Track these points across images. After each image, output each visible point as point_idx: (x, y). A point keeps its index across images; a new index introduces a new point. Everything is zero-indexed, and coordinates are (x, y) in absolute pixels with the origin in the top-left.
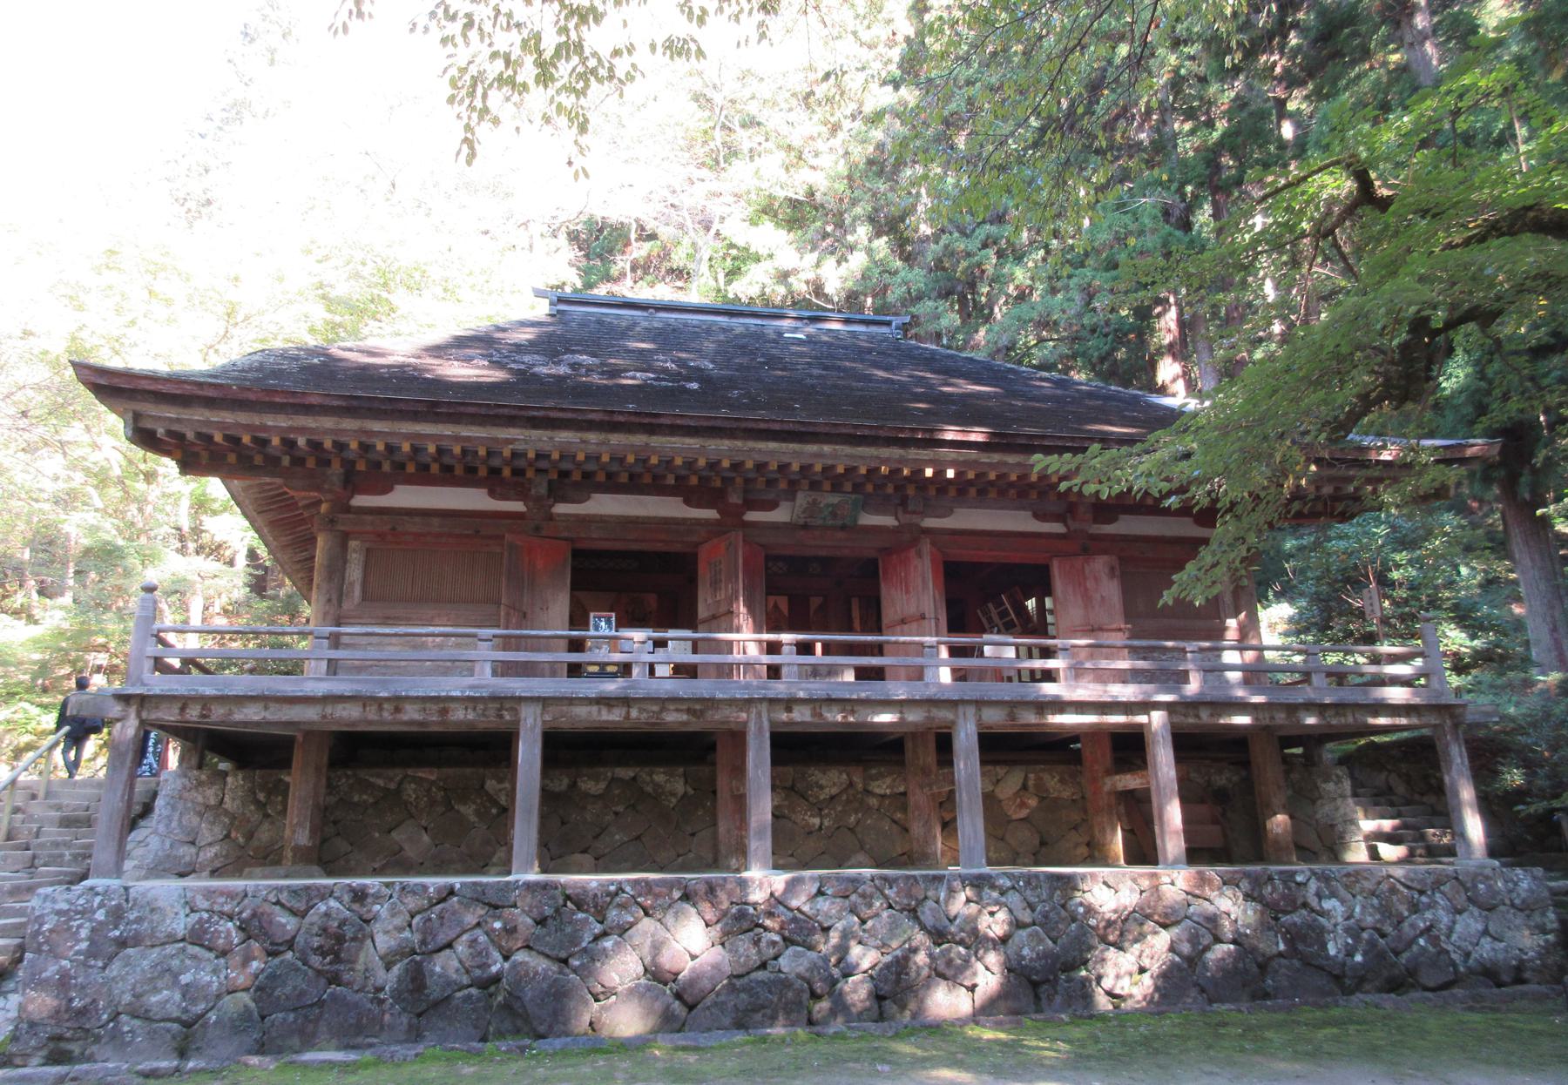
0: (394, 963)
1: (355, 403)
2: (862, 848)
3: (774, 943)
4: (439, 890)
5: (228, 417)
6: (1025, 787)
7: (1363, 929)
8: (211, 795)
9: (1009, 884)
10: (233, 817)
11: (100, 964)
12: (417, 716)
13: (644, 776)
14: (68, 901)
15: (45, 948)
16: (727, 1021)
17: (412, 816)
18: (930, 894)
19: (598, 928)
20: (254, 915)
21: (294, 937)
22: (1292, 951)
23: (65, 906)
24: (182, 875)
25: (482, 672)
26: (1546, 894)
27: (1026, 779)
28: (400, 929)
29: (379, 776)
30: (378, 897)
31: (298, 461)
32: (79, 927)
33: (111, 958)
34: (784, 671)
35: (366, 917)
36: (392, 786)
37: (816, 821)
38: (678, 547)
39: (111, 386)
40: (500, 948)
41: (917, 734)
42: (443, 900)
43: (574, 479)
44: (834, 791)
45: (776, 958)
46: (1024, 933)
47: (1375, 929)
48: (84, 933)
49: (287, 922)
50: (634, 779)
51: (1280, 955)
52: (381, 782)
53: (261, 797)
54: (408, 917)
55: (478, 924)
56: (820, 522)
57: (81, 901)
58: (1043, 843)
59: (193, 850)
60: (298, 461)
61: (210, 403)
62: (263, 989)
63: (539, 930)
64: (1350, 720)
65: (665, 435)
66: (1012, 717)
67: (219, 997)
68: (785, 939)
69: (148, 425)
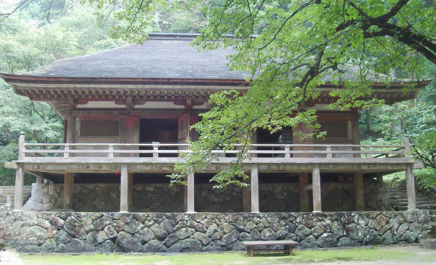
2: (231, 208)
3: (192, 231)
5: (39, 85)
6: (283, 190)
7: (370, 229)
8: (45, 190)
9: (262, 216)
12: (93, 168)
16: (178, 251)
17: (98, 197)
20: (53, 219)
26: (429, 218)
27: (284, 187)
31: (59, 96)
36: (93, 188)
37: (217, 199)
40: (116, 230)
41: (303, 174)
43: (139, 98)
49: (62, 221)
50: (162, 187)
51: (344, 236)
52: (90, 187)
53: (58, 190)
54: (92, 221)
55: (110, 224)
58: (288, 206)
59: (42, 205)
60: (59, 96)
65: (161, 85)
66: (269, 167)
67: (46, 239)
69: (19, 88)
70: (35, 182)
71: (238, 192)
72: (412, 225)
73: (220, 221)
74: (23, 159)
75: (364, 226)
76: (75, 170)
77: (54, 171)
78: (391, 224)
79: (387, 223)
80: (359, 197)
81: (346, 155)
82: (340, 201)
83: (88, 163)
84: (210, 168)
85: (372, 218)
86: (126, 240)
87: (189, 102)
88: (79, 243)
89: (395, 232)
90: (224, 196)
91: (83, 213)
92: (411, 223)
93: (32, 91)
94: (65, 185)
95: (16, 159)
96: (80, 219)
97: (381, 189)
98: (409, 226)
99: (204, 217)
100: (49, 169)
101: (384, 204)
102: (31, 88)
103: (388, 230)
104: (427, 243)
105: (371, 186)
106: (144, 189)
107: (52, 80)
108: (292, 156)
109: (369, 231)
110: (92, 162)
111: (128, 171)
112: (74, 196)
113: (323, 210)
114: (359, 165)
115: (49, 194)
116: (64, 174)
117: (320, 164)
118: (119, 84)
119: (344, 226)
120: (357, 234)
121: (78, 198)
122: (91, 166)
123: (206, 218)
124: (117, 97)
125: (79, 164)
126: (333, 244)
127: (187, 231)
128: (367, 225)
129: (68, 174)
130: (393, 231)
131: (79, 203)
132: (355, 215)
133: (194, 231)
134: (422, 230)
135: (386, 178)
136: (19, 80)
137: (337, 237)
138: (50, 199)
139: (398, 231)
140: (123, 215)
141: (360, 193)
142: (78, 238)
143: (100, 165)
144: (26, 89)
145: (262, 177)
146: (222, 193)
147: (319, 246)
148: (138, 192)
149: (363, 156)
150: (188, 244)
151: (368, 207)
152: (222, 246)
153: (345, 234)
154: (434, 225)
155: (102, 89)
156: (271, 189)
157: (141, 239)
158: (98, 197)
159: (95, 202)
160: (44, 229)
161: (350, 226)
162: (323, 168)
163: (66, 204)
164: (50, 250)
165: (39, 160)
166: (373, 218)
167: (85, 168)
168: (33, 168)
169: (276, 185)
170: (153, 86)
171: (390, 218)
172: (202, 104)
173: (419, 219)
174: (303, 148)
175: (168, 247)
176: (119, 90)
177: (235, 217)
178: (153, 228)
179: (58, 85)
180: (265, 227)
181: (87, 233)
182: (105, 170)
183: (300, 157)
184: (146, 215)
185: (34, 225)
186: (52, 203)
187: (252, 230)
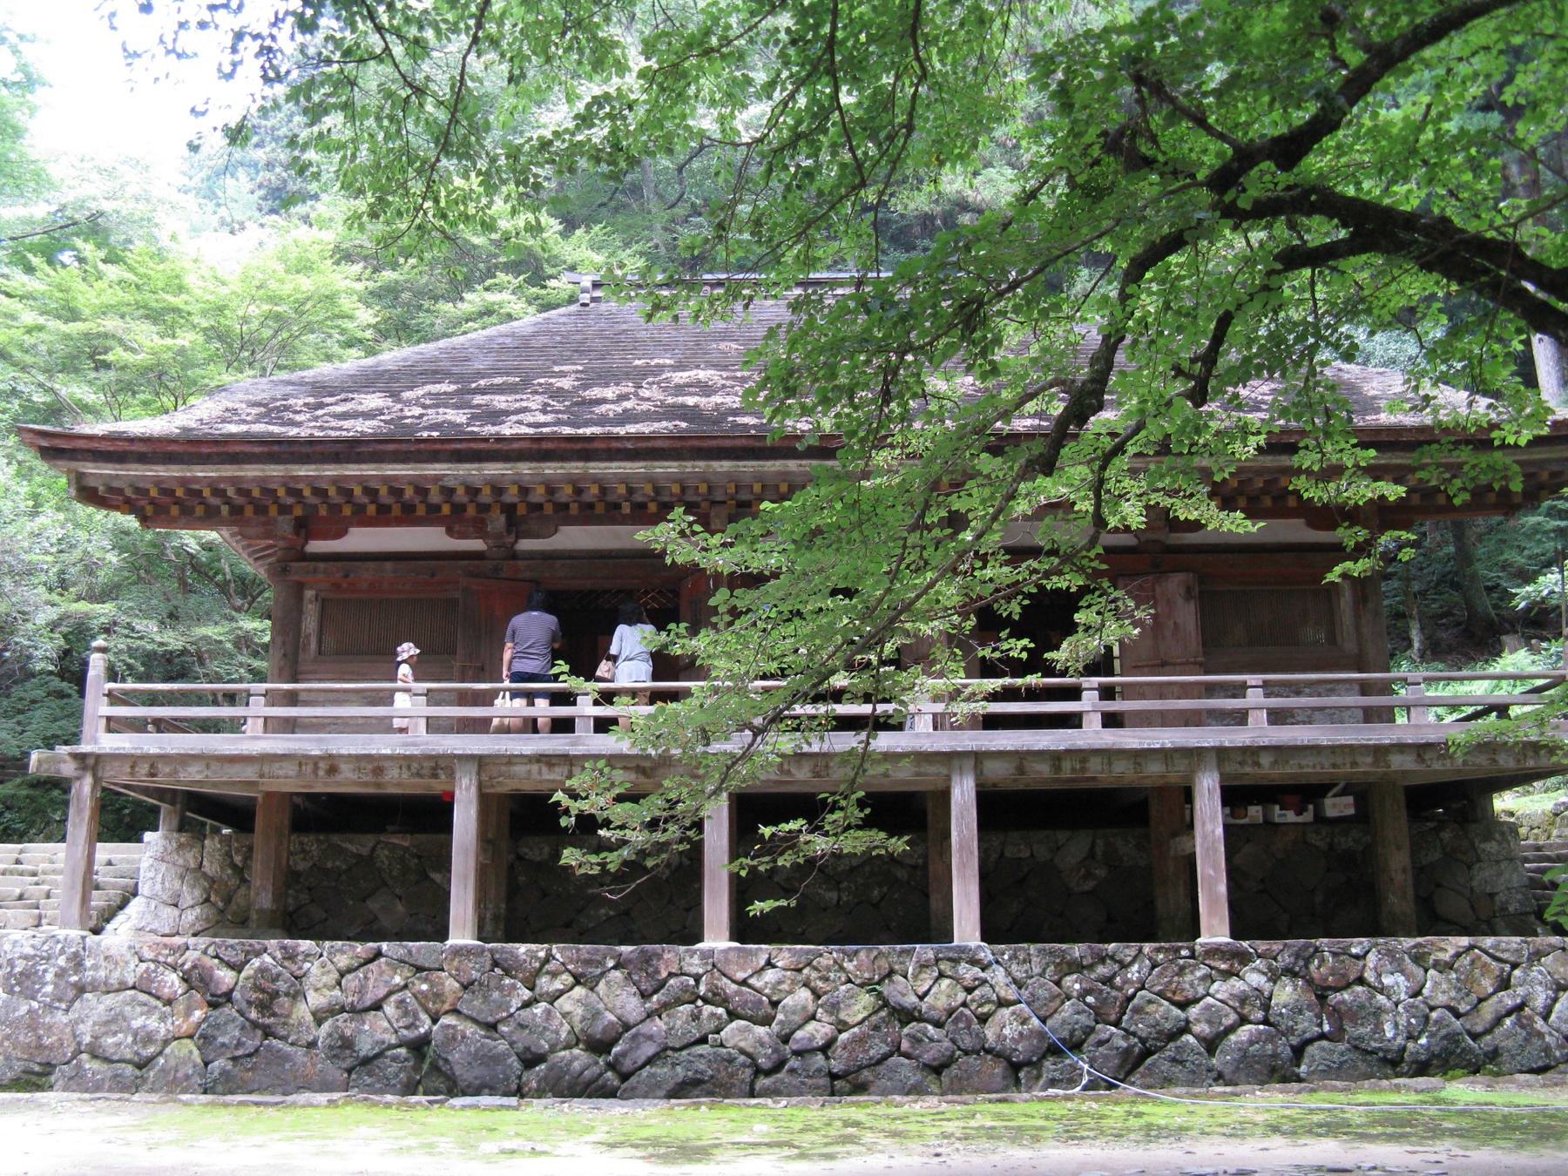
0: (326, 1019)
1: (276, 448)
5: (161, 471)
6: (1091, 855)
7: (1432, 1009)
8: (190, 858)
10: (212, 881)
11: (64, 1006)
14: (33, 946)
15: (17, 989)
16: (663, 1093)
20: (195, 967)
21: (232, 990)
23: (32, 952)
28: (331, 988)
29: (351, 842)
31: (236, 511)
32: (45, 971)
33: (72, 1002)
35: (299, 973)
36: (365, 852)
37: (834, 895)
40: (427, 1011)
41: (1163, 791)
43: (526, 512)
48: (49, 977)
49: (225, 977)
51: (1322, 1036)
52: (353, 848)
54: (336, 975)
55: (406, 986)
57: (46, 947)
59: (176, 912)
61: (169, 458)
66: (1021, 770)
67: (166, 1043)
68: (729, 1013)
69: (92, 483)
70: (156, 829)
71: (915, 867)
73: (826, 979)
74: (95, 741)
75: (1403, 996)
76: (288, 781)
77: (215, 784)
78: (1520, 991)
79: (1504, 984)
83: (331, 756)
84: (789, 772)
85: (1436, 965)
86: (463, 1048)
88: (286, 1058)
89: (1539, 1024)
90: (860, 881)
91: (306, 945)
93: (138, 490)
94: (258, 838)
95: (73, 738)
96: (294, 968)
97: (1491, 847)
99: (762, 963)
100: (192, 777)
101: (1504, 909)
102: (149, 482)
103: (1509, 1014)
105: (1446, 835)
107: (205, 450)
109: (1427, 1018)
110: (344, 752)
111: (480, 787)
112: (289, 879)
113: (1234, 935)
115: (205, 874)
116: (254, 799)
117: (1221, 753)
118: (449, 461)
119: (1322, 998)
120: (1378, 1028)
121: (310, 889)
122: (343, 767)
123: (770, 964)
124: (446, 509)
125: (301, 760)
126: (1279, 1068)
127: (696, 1017)
129: (269, 795)
130: (1530, 1018)
131: (307, 912)
132: (1369, 953)
133: (725, 1016)
135: (1505, 802)
136: (88, 451)
137: (1294, 1041)
138: (207, 892)
139: (1553, 1017)
140: (457, 952)
141: (1397, 862)
142: (284, 1038)
143: (376, 764)
144: (116, 484)
145: (992, 805)
146: (852, 869)
147: (1219, 1078)
149: (1401, 719)
151: (1433, 922)
152: (833, 1076)
153: (1326, 1028)
155: (385, 479)
156: (1042, 853)
158: (385, 884)
159: (374, 905)
160: (159, 1004)
162: (1231, 768)
163: (261, 911)
164: (173, 1085)
165: (152, 743)
166: (1445, 967)
167: (321, 773)
168: (132, 774)
169: (1062, 836)
170: (575, 468)
171: (1515, 966)
175: (625, 1077)
176: (451, 484)
177: (884, 964)
178: (564, 1003)
179: (229, 471)
180: (1002, 1003)
181: (319, 1023)
182: (397, 783)
183: (1150, 725)
184: (542, 954)
185: (123, 987)
186: (214, 904)
187: (950, 1012)
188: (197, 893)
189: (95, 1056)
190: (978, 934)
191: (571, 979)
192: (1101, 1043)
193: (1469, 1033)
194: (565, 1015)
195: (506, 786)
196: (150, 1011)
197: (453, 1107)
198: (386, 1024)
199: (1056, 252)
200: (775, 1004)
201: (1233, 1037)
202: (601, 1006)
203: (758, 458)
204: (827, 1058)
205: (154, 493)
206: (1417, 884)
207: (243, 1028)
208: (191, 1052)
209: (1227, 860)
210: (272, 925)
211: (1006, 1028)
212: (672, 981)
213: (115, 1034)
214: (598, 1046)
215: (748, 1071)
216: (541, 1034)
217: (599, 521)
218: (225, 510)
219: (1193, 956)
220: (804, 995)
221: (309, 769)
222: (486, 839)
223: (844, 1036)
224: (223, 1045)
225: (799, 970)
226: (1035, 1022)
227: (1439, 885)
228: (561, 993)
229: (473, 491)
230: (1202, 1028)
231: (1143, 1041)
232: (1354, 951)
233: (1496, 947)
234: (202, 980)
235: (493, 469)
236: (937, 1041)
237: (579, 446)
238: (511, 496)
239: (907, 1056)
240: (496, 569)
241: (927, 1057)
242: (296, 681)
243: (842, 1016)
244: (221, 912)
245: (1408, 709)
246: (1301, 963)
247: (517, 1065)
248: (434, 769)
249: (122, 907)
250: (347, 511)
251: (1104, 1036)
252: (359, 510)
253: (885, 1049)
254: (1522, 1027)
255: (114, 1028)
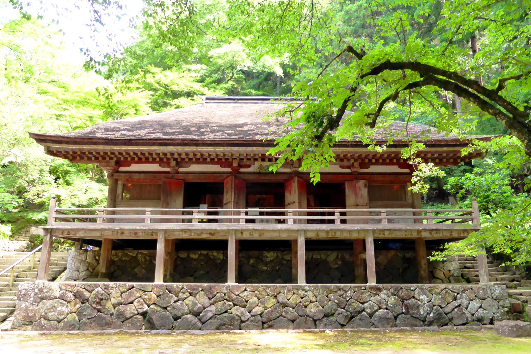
3: (229, 305)
4: (129, 286)
6: (337, 257)
7: (434, 306)
8: (83, 257)
9: (308, 289)
10: (89, 264)
13: (210, 253)
15: (22, 299)
16: (213, 328)
18: (282, 291)
19: (176, 299)
20: (77, 291)
22: (407, 313)
23: (27, 288)
24: (75, 280)
25: (147, 221)
26: (506, 294)
27: (338, 256)
28: (118, 297)
30: (112, 288)
31: (97, 158)
34: (241, 220)
36: (134, 255)
37: (265, 268)
38: (218, 181)
39: (40, 139)
40: (146, 304)
41: (357, 240)
42: (130, 289)
43: (181, 162)
44: (272, 259)
45: (230, 309)
46: (313, 304)
47: (439, 305)
48: (32, 295)
49: (87, 294)
50: (207, 254)
51: (403, 313)
54: (120, 293)
55: (141, 297)
56: (264, 172)
58: (342, 276)
59: (78, 273)
62: (79, 313)
63: (158, 299)
64: (441, 235)
66: (318, 235)
67: (68, 314)
68: (234, 304)
72: (484, 301)
73: (261, 294)
78: (460, 301)
79: (455, 299)
80: (422, 267)
81: (405, 221)
82: (401, 271)
84: (252, 235)
87: (235, 165)
88: (104, 318)
92: (484, 299)
96: (108, 291)
98: (482, 303)
99: (243, 289)
103: (456, 307)
104: (503, 327)
106: (188, 256)
108: (343, 221)
110: (126, 228)
112: (110, 263)
114: (419, 232)
123: (245, 290)
125: (113, 231)
127: (224, 305)
128: (430, 301)
129: (105, 240)
130: (462, 309)
131: (114, 274)
134: (499, 308)
139: (469, 309)
140: (156, 286)
142: (103, 313)
143: (136, 232)
144: (59, 150)
145: (310, 244)
148: (183, 259)
149: (425, 222)
150: (226, 319)
152: (263, 323)
153: (404, 311)
154: (512, 302)
155: (140, 150)
156: (323, 257)
157: (173, 314)
159: (136, 270)
160: (66, 303)
161: (410, 301)
163: (102, 273)
169: (329, 252)
170: (194, 148)
171: (458, 294)
172: (249, 166)
173: (493, 295)
174: (357, 213)
175: (203, 323)
180: (311, 302)
181: (114, 308)
182: (142, 236)
184: (180, 287)
188: (85, 267)
189: (45, 319)
190: (305, 281)
191: (189, 294)
192: (339, 314)
193: (445, 313)
194: (187, 305)
195: (173, 238)
196: (63, 305)
197: (151, 334)
198: (134, 308)
199: (324, 72)
200: (247, 302)
201: (377, 313)
202: (197, 302)
203: (245, 147)
204: (261, 317)
205: (71, 153)
206: (429, 267)
207: (91, 309)
208: (75, 317)
209: (375, 259)
210: (105, 277)
211: (312, 309)
212: (218, 295)
213: (51, 312)
214: (197, 314)
215: (239, 321)
216: (179, 310)
217: (208, 163)
218: (93, 158)
219: (365, 289)
220: (255, 299)
221: (115, 233)
222: (167, 253)
223: (266, 311)
224: (85, 315)
225: (254, 292)
226: (321, 307)
227: (434, 268)
228: (186, 298)
229: (165, 154)
230: (369, 311)
231: (351, 313)
232: (412, 288)
233: (453, 288)
234: (79, 296)
235: (171, 148)
236: (291, 313)
237: (194, 142)
238: (176, 156)
239: (284, 317)
240: (173, 176)
241: (289, 317)
242: (115, 207)
243: (266, 305)
244: (92, 273)
245: (427, 219)
246: (397, 292)
247: (172, 319)
248: (152, 233)
249: (64, 271)
250: (129, 159)
251: (341, 312)
252: (133, 159)
253: (278, 315)
254: (460, 311)
255: (52, 310)
